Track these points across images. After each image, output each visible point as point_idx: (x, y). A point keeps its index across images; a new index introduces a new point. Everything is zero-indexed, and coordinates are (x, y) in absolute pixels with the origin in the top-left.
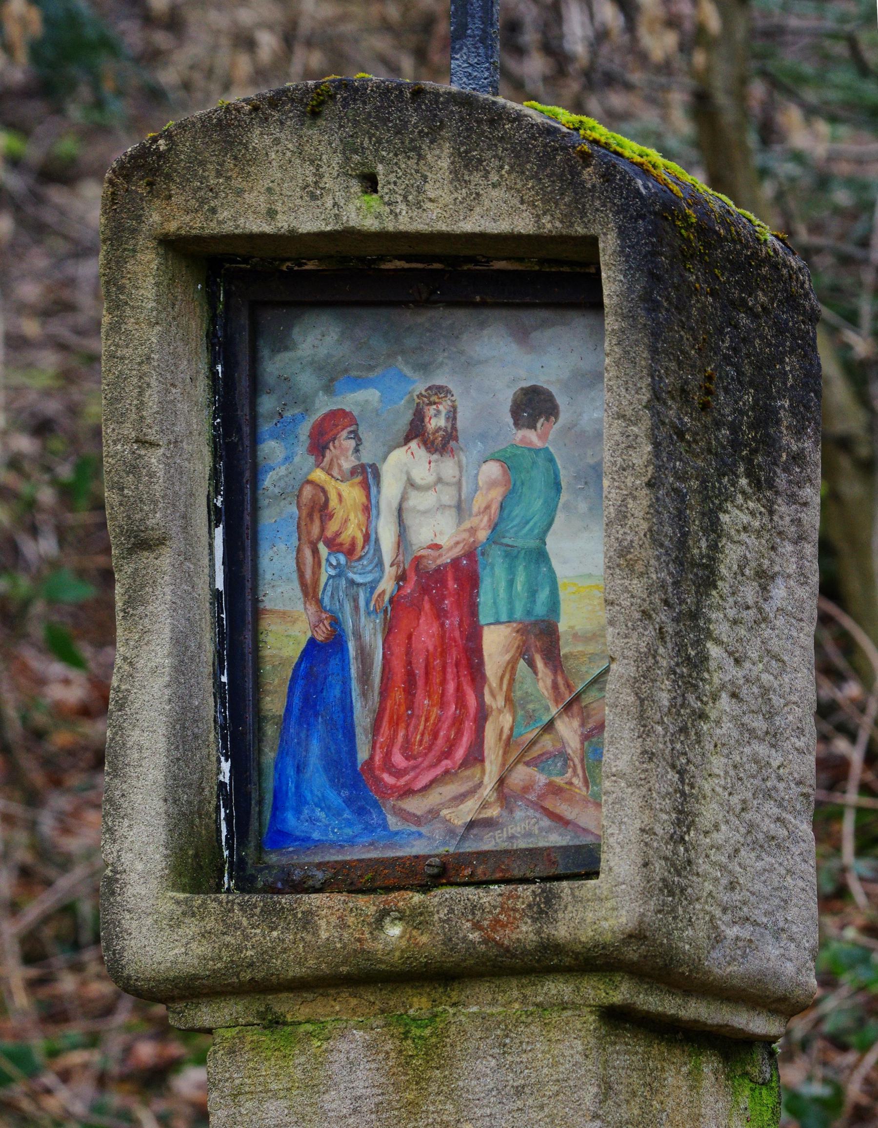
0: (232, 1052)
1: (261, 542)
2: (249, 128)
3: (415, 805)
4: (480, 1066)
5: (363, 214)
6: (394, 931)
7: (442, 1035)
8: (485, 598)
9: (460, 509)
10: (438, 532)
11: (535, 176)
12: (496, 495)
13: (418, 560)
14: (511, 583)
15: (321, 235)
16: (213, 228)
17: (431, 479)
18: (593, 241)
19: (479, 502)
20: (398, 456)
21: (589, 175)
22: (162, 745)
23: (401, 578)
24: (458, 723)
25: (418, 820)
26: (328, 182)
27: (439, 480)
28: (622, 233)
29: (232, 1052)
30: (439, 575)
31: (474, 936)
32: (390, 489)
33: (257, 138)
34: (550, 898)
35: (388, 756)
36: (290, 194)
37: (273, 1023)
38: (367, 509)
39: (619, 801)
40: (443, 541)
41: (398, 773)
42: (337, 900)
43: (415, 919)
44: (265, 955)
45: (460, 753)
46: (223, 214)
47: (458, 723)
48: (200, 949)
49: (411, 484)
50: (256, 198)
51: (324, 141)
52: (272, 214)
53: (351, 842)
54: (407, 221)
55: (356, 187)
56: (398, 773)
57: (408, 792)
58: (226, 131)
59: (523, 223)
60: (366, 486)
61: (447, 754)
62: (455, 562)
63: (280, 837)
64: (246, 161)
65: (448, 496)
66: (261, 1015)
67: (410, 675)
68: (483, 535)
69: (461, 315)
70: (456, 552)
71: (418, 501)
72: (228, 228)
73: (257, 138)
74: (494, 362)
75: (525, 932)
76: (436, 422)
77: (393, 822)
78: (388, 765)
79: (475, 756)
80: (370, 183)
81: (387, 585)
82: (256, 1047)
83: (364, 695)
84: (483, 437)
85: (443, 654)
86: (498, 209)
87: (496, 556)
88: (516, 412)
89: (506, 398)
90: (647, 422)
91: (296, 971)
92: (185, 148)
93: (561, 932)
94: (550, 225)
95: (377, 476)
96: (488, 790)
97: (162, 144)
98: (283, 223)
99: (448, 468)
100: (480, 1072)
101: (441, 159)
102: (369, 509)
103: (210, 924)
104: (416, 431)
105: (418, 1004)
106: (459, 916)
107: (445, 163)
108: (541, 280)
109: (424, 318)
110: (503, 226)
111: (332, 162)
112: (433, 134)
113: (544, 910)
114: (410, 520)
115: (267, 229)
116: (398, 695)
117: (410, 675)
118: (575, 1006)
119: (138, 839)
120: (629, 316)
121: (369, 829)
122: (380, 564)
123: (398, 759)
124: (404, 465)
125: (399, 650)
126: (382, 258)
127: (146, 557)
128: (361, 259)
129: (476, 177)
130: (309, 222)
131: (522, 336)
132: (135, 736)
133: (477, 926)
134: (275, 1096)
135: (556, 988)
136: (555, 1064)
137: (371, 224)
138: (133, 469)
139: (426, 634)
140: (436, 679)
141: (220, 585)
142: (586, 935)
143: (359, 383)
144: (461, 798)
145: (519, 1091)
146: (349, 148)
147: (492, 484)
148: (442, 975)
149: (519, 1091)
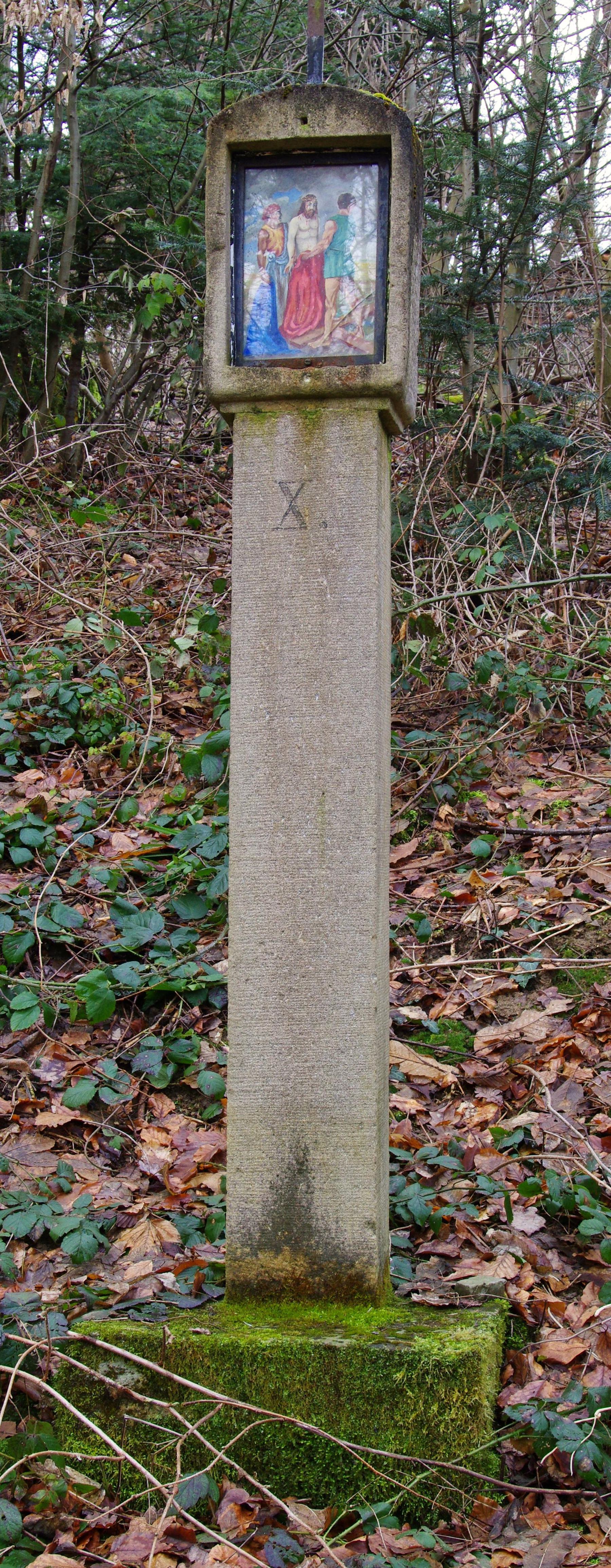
0: (243, 421)
1: (246, 251)
2: (261, 104)
3: (298, 341)
4: (333, 429)
5: (302, 131)
6: (307, 381)
7: (319, 418)
8: (326, 269)
9: (318, 238)
10: (310, 246)
11: (368, 114)
12: (331, 232)
13: (301, 257)
14: (336, 264)
15: (286, 140)
16: (247, 139)
17: (307, 227)
18: (388, 138)
19: (324, 237)
20: (295, 220)
21: (389, 113)
22: (224, 316)
23: (295, 262)
24: (315, 312)
25: (299, 346)
26: (290, 121)
27: (310, 228)
28: (401, 133)
29: (243, 421)
30: (309, 261)
31: (339, 383)
32: (292, 231)
33: (264, 107)
34: (368, 370)
35: (289, 324)
36: (277, 125)
37: (257, 412)
38: (283, 239)
39: (395, 336)
40: (311, 249)
41: (292, 330)
42: (287, 370)
43: (316, 377)
44: (261, 387)
45: (316, 323)
46: (251, 134)
47: (315, 312)
48: (238, 385)
49: (300, 229)
50: (263, 128)
51: (289, 107)
52: (268, 133)
53: (275, 353)
54: (318, 133)
55: (299, 122)
56: (292, 330)
57: (296, 337)
58: (253, 106)
59: (363, 132)
60: (283, 231)
61: (311, 323)
62: (316, 256)
63: (248, 352)
64: (260, 115)
65: (313, 233)
66: (254, 409)
67: (298, 296)
68: (326, 247)
69: (320, 169)
70: (317, 252)
71: (303, 235)
72: (253, 139)
73: (264, 107)
74: (330, 185)
75: (358, 382)
76: (309, 207)
77: (290, 347)
78: (289, 327)
79: (321, 324)
80: (304, 121)
81: (290, 265)
82: (252, 420)
83: (281, 302)
84: (327, 212)
85: (310, 288)
86: (353, 126)
87: (331, 254)
88: (340, 203)
89: (336, 197)
90: (408, 201)
91: (271, 393)
92: (238, 112)
93: (372, 381)
94: (373, 132)
95: (287, 226)
96: (326, 336)
97: (230, 111)
98: (273, 136)
99: (314, 223)
100: (333, 431)
101: (332, 111)
102: (284, 239)
103: (242, 376)
104: (302, 210)
105: (310, 407)
106: (332, 377)
107: (333, 112)
108: (367, 153)
109: (306, 171)
110: (355, 133)
111: (291, 114)
112: (329, 102)
113: (366, 373)
114: (298, 242)
115: (267, 138)
116: (293, 303)
117: (298, 296)
118: (370, 409)
119: (217, 348)
120: (403, 163)
121: (281, 349)
122: (288, 258)
123: (293, 325)
124: (297, 223)
125: (294, 287)
126: (294, 150)
127: (218, 253)
128: (286, 151)
129: (345, 116)
130: (282, 135)
131: (343, 177)
132: (215, 313)
133: (340, 379)
134: (258, 436)
135: (362, 403)
136: (362, 429)
137: (305, 135)
138: (216, 223)
139: (304, 281)
140: (307, 297)
141: (232, 265)
142: (381, 383)
143: (281, 195)
144: (316, 339)
145: (348, 438)
146: (298, 108)
147: (330, 229)
148: (320, 397)
149: (348, 438)
